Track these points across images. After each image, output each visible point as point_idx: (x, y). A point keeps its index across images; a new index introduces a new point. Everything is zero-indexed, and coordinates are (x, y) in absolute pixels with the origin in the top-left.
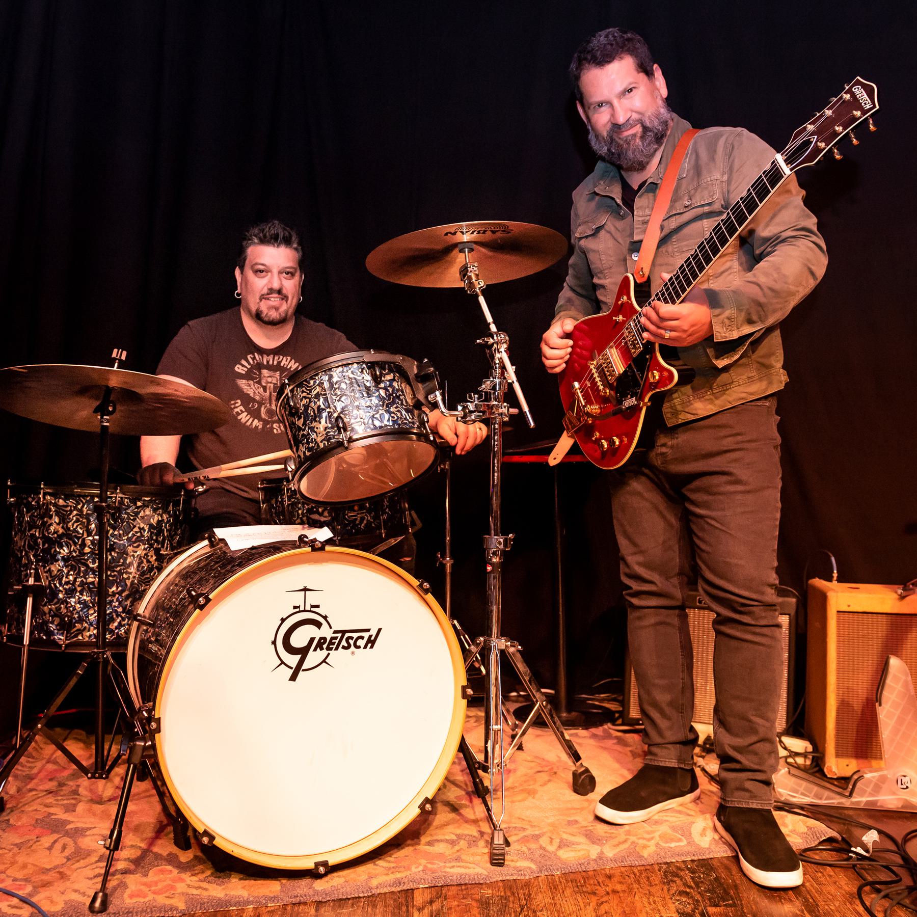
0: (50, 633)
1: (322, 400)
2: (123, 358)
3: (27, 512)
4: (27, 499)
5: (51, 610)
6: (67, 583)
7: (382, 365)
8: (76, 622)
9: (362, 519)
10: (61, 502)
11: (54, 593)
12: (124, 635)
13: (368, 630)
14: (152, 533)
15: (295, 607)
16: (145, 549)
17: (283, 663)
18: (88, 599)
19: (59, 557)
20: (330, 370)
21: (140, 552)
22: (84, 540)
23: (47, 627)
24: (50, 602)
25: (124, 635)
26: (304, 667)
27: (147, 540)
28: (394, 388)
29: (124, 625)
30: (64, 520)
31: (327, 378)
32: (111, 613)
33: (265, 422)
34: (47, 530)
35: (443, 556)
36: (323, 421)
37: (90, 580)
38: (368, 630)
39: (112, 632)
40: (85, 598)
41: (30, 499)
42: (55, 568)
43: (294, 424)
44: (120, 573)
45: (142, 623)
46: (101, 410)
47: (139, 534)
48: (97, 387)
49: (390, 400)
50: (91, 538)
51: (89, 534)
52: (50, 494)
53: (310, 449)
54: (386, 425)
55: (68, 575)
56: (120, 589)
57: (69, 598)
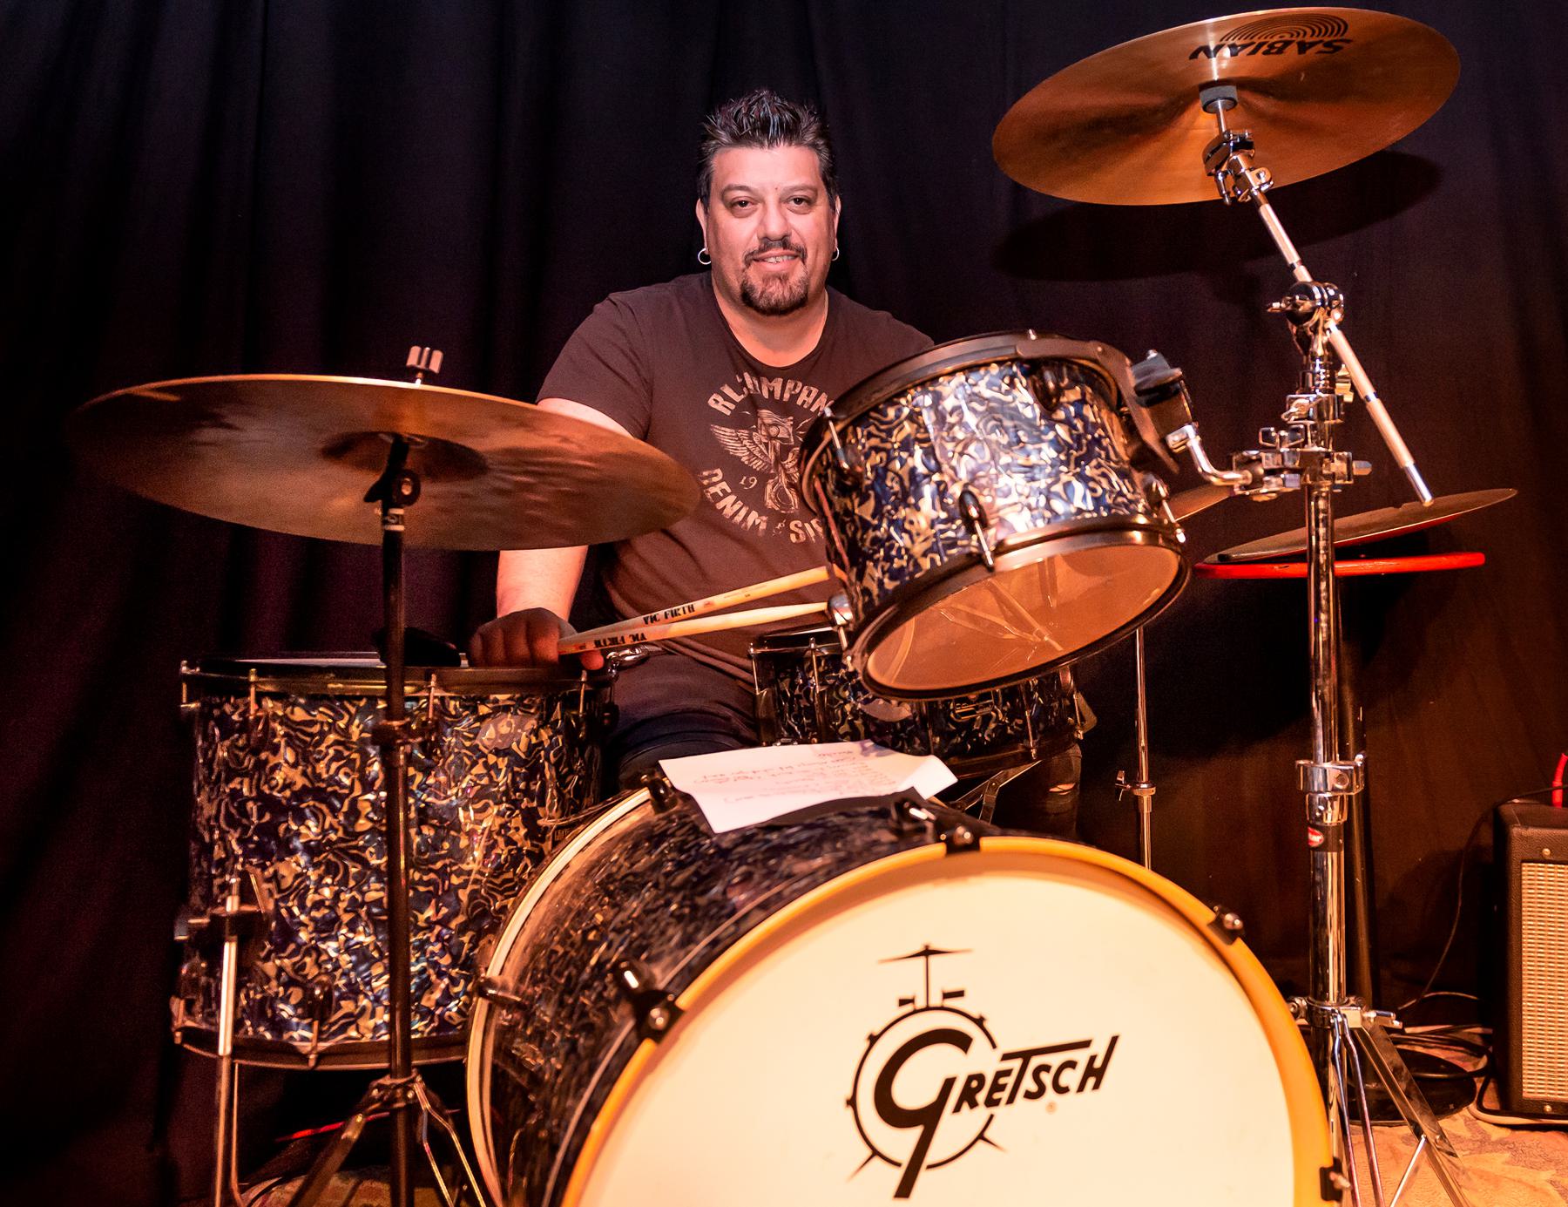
0: (279, 1026)
1: (918, 452)
2: (435, 366)
3: (223, 738)
4: (220, 706)
5: (280, 969)
6: (318, 905)
7: (1056, 363)
8: (343, 997)
9: (987, 719)
10: (299, 714)
11: (287, 932)
12: (457, 1019)
13: (1085, 1044)
14: (515, 774)
15: (903, 1002)
16: (500, 814)
17: (875, 1153)
18: (368, 940)
19: (298, 843)
20: (934, 380)
21: (490, 821)
22: (354, 801)
23: (274, 1009)
24: (279, 949)
25: (457, 1019)
26: (930, 1158)
27: (506, 793)
28: (1084, 419)
29: (457, 996)
30: (305, 756)
31: (928, 400)
32: (424, 970)
33: (775, 517)
34: (267, 782)
35: (1133, 779)
36: (926, 503)
37: (372, 896)
38: (1085, 1044)
39: (427, 1014)
40: (361, 938)
41: (228, 708)
42: (289, 869)
43: (849, 513)
44: (444, 874)
45: (496, 1003)
46: (383, 494)
47: (485, 781)
48: (371, 436)
49: (1080, 451)
50: (371, 796)
51: (368, 786)
52: (273, 696)
53: (895, 574)
54: (1080, 511)
55: (319, 884)
56: (444, 911)
57: (324, 940)
